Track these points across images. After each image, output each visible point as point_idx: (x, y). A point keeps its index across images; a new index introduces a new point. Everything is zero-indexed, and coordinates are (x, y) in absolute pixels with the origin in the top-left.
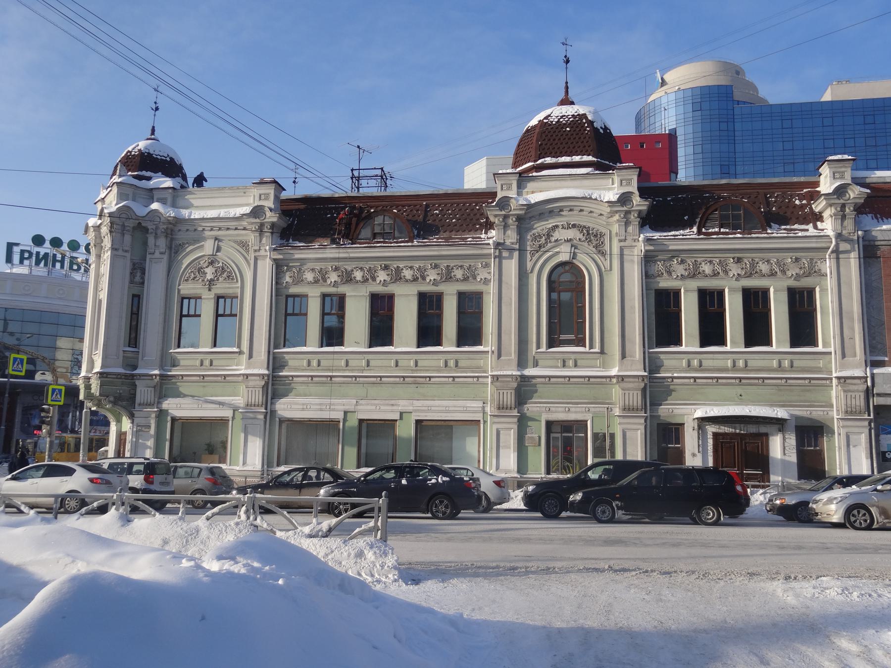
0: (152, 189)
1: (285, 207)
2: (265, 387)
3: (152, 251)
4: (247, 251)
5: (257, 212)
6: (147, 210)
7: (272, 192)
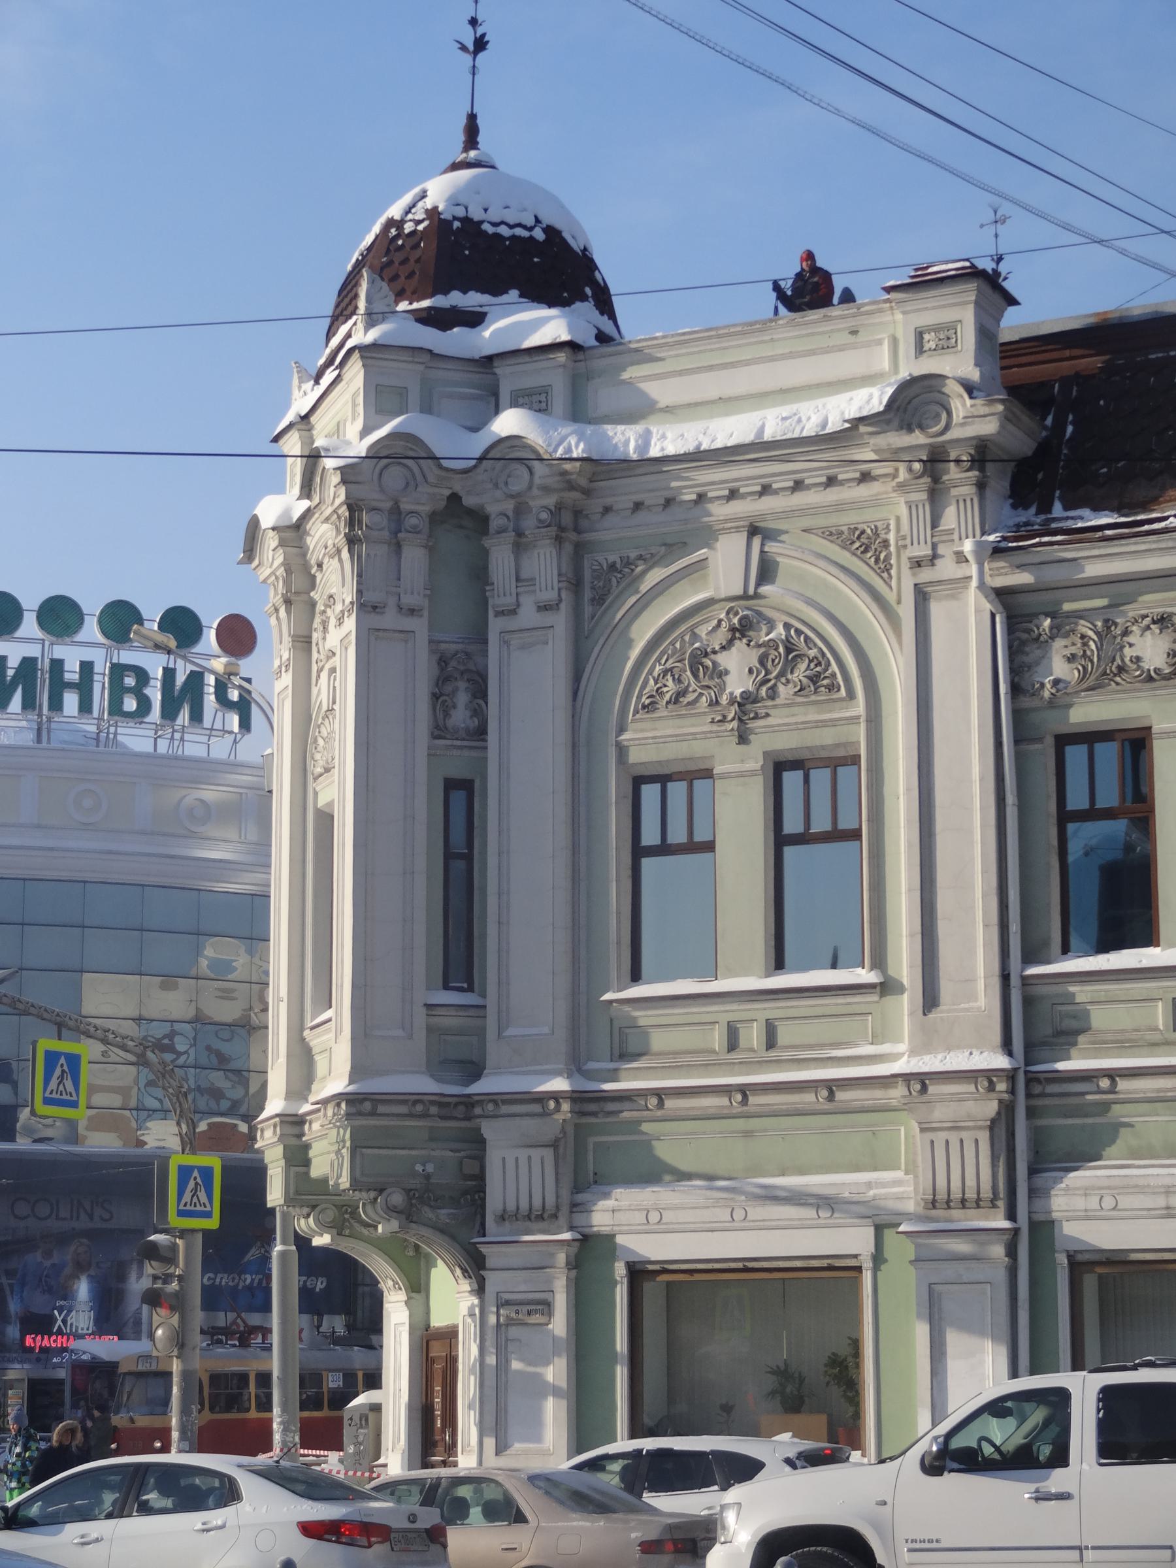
0: (490, 359)
1: (1021, 374)
2: (1002, 1126)
3: (508, 601)
4: (884, 568)
5: (913, 403)
6: (477, 444)
7: (966, 318)
